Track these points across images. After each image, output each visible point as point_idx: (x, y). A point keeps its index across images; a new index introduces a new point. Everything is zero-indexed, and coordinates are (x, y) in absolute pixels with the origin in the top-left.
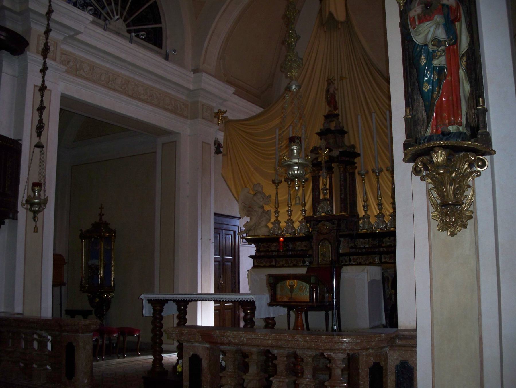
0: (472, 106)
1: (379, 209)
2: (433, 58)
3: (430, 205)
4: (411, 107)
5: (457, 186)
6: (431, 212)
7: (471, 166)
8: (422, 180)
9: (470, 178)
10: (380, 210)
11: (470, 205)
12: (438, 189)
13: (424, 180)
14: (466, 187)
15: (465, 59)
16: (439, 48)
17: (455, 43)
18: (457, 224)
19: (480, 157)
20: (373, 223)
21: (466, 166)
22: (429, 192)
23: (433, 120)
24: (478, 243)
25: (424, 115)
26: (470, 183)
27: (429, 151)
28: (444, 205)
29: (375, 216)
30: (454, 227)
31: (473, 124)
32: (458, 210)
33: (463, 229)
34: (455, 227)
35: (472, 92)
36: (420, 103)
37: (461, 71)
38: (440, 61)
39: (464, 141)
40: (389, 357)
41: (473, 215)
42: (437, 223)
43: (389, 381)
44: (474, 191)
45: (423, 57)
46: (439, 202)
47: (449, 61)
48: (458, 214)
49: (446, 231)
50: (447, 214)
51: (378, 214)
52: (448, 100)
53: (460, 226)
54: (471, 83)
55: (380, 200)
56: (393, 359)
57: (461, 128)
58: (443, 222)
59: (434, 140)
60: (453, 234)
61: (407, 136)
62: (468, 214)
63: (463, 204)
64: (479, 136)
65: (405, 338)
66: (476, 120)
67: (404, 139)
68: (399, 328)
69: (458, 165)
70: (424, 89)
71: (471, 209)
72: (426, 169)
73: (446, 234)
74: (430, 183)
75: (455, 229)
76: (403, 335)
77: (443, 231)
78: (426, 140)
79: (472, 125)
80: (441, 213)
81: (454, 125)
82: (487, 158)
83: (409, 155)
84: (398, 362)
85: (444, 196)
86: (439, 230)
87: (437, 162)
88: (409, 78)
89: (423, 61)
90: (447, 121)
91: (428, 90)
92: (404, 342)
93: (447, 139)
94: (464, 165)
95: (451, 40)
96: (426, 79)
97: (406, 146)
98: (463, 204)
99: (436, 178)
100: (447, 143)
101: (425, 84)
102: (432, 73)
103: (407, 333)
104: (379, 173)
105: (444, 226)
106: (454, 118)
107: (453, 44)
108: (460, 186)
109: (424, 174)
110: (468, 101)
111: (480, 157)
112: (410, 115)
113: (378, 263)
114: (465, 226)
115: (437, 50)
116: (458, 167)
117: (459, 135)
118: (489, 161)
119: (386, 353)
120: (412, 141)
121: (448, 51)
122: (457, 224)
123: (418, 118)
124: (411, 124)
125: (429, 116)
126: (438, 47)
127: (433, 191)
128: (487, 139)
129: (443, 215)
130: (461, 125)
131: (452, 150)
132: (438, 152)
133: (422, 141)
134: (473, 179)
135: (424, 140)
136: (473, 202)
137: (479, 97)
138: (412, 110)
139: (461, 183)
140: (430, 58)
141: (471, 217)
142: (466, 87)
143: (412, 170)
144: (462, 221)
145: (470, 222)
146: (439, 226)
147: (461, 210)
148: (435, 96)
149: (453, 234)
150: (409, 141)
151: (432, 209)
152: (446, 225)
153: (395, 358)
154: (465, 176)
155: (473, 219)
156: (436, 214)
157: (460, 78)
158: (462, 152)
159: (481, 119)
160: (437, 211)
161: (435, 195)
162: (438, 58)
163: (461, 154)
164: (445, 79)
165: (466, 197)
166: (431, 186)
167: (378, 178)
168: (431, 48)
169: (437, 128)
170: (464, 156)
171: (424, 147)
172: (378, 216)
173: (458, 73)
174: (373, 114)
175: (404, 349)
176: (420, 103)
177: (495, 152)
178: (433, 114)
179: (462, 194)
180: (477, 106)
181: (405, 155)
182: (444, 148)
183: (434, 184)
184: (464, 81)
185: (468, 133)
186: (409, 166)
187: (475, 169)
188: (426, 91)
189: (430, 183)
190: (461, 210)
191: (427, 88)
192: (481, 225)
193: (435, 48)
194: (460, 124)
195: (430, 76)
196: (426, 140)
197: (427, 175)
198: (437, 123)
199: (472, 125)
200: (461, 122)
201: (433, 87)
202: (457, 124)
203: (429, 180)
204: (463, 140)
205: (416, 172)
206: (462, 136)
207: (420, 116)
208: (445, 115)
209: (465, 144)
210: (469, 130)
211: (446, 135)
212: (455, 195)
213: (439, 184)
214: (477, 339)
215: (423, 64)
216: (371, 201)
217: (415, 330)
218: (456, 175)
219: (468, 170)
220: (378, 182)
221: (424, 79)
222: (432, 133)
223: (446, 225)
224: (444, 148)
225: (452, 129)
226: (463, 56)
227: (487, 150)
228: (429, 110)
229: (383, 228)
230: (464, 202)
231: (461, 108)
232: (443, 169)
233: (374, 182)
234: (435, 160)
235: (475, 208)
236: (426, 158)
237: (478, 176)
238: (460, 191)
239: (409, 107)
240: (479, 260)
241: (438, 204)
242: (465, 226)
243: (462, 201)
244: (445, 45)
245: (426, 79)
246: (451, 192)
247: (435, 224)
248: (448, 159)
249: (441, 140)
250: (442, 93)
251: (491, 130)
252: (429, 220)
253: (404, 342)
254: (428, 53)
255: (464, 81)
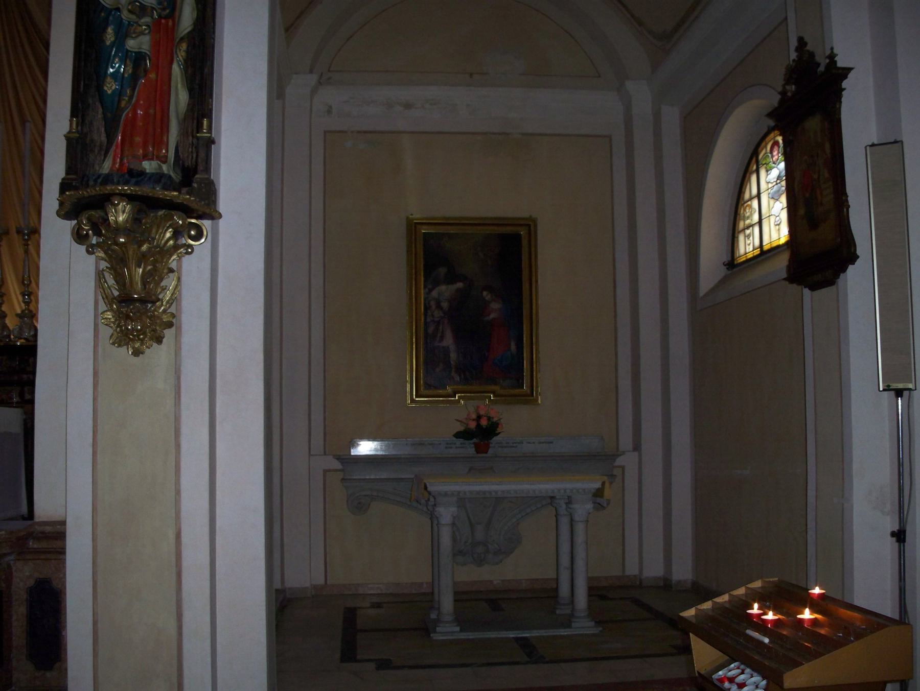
0: (190, 130)
1: (24, 302)
2: (127, 35)
3: (100, 297)
4: (80, 118)
5: (149, 267)
6: (100, 311)
7: (176, 235)
8: (88, 252)
9: (175, 257)
10: (27, 304)
11: (170, 303)
12: (115, 270)
13: (93, 253)
14: (165, 271)
15: (184, 46)
16: (140, 19)
17: (171, 15)
18: (144, 334)
19: (193, 221)
20: (11, 328)
21: (168, 235)
22: (100, 275)
23: (117, 146)
24: (180, 369)
25: (104, 138)
26: (173, 265)
27: (102, 202)
28: (125, 299)
29: (17, 315)
30: (139, 339)
31: (188, 163)
32: (147, 311)
33: (155, 345)
34: (142, 340)
35: (191, 107)
36: (97, 116)
37: (175, 67)
38: (140, 43)
39: (167, 190)
40: (14, 574)
41: (174, 321)
42: (110, 331)
43: (14, 618)
44: (179, 279)
45: (110, 30)
46: (116, 293)
47: (156, 45)
48: (148, 317)
49: (125, 347)
50: (128, 317)
51: (23, 311)
52: (146, 114)
53: (151, 339)
54: (191, 91)
55: (29, 285)
56: (24, 574)
57: (165, 167)
58: (121, 331)
59: (113, 183)
60: (137, 353)
61: (68, 172)
62: (165, 318)
63: (159, 300)
64: (195, 185)
65: (45, 536)
66: (195, 156)
67: (62, 174)
68: (37, 519)
69: (154, 231)
70: (105, 88)
71: (173, 310)
72: (98, 233)
73: (125, 352)
74: (103, 259)
75: (142, 344)
76: (43, 533)
77: (120, 346)
78: (99, 181)
79: (186, 164)
80: (118, 315)
81: (152, 159)
82: (206, 224)
83: (68, 205)
84: (31, 582)
85: (124, 284)
86: (113, 344)
87: (116, 222)
88: (83, 64)
89: (108, 37)
90: (141, 151)
91: (114, 91)
92: (43, 545)
93: (137, 184)
94: (165, 233)
95: (164, 9)
96: (111, 70)
97: (64, 187)
98: (159, 300)
99: (113, 251)
100: (135, 191)
101: (109, 79)
102: (123, 61)
103: (48, 529)
104: (28, 235)
105: (123, 338)
106: (153, 148)
107: (166, 18)
108: (155, 269)
109: (94, 242)
110: (183, 123)
111: (193, 221)
112: (77, 132)
113: (17, 403)
114: (159, 340)
115: (137, 23)
116: (153, 235)
117: (158, 178)
118: (209, 229)
119: (9, 566)
120: (75, 180)
121: (156, 27)
122: (144, 334)
123: (92, 141)
124: (78, 149)
125: (110, 138)
126: (140, 17)
127: (107, 275)
128: (209, 193)
129: (122, 317)
130: (164, 162)
131: (145, 205)
132: (118, 204)
133: (91, 183)
134: (180, 258)
135: (95, 181)
136: (175, 299)
137: (203, 116)
138: (82, 123)
139: (159, 263)
140: (123, 33)
141: (170, 325)
142: (180, 97)
143: (72, 234)
144: (154, 331)
145: (169, 334)
146: (114, 337)
147: (155, 310)
148: (123, 104)
149: (137, 353)
150: (71, 179)
151: (102, 306)
152: (127, 335)
153: (27, 574)
154: (165, 252)
155: (174, 328)
156: (109, 315)
157: (173, 79)
158: (163, 208)
159: (202, 154)
160: (111, 310)
161: (111, 281)
162: (136, 37)
163: (161, 213)
164: (145, 76)
165: (164, 289)
166: (104, 265)
167: (28, 245)
168: (125, 15)
169: (121, 160)
170: (165, 216)
171: (94, 193)
172: (21, 316)
173: (171, 68)
174: (28, 124)
175: (43, 557)
176: (97, 116)
177: (220, 216)
178: (117, 137)
179: (158, 284)
180: (198, 132)
181: (61, 204)
182: (130, 198)
183: (110, 262)
184: (179, 86)
185: (176, 177)
186: (69, 225)
187: (184, 242)
188: (109, 92)
189: (103, 259)
190: (155, 310)
191: (110, 87)
192: (187, 339)
193: (134, 17)
194: (164, 160)
195: (120, 67)
196: (99, 181)
197: (98, 245)
198: (122, 151)
199: (186, 164)
200: (166, 157)
201: (122, 86)
202: (158, 158)
203: (102, 254)
204: (165, 188)
205: (79, 237)
206: (163, 181)
207: (95, 137)
208: (138, 139)
209: (166, 195)
210: (179, 172)
211: (137, 176)
212: (145, 283)
213: (118, 262)
214: (171, 535)
215: (108, 43)
216: (11, 286)
217: (63, 523)
218: (149, 249)
219: (171, 242)
220: (27, 252)
221: (107, 69)
222: (111, 169)
223: (127, 335)
224: (130, 198)
225: (148, 166)
226: (182, 39)
227: (207, 211)
228: (111, 128)
229: (31, 339)
230: (161, 297)
231: (168, 131)
232: (126, 236)
233: (20, 251)
234: (112, 218)
235: (179, 309)
236: (96, 214)
237: (188, 253)
238: (155, 276)
239: (77, 117)
240: (179, 399)
241: (115, 298)
242: (159, 340)
243: (157, 296)
244: (152, 17)
245: (111, 70)
246: (138, 279)
247: (106, 332)
248: (136, 219)
249: (126, 183)
250: (138, 101)
251: (218, 178)
252: (96, 325)
253: (43, 545)
254: (119, 24)
255: (179, 86)
